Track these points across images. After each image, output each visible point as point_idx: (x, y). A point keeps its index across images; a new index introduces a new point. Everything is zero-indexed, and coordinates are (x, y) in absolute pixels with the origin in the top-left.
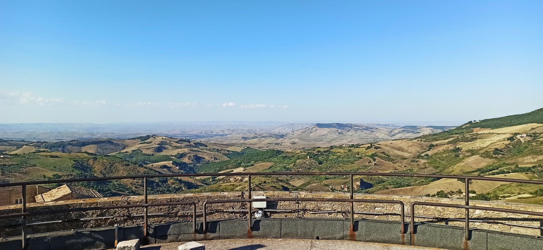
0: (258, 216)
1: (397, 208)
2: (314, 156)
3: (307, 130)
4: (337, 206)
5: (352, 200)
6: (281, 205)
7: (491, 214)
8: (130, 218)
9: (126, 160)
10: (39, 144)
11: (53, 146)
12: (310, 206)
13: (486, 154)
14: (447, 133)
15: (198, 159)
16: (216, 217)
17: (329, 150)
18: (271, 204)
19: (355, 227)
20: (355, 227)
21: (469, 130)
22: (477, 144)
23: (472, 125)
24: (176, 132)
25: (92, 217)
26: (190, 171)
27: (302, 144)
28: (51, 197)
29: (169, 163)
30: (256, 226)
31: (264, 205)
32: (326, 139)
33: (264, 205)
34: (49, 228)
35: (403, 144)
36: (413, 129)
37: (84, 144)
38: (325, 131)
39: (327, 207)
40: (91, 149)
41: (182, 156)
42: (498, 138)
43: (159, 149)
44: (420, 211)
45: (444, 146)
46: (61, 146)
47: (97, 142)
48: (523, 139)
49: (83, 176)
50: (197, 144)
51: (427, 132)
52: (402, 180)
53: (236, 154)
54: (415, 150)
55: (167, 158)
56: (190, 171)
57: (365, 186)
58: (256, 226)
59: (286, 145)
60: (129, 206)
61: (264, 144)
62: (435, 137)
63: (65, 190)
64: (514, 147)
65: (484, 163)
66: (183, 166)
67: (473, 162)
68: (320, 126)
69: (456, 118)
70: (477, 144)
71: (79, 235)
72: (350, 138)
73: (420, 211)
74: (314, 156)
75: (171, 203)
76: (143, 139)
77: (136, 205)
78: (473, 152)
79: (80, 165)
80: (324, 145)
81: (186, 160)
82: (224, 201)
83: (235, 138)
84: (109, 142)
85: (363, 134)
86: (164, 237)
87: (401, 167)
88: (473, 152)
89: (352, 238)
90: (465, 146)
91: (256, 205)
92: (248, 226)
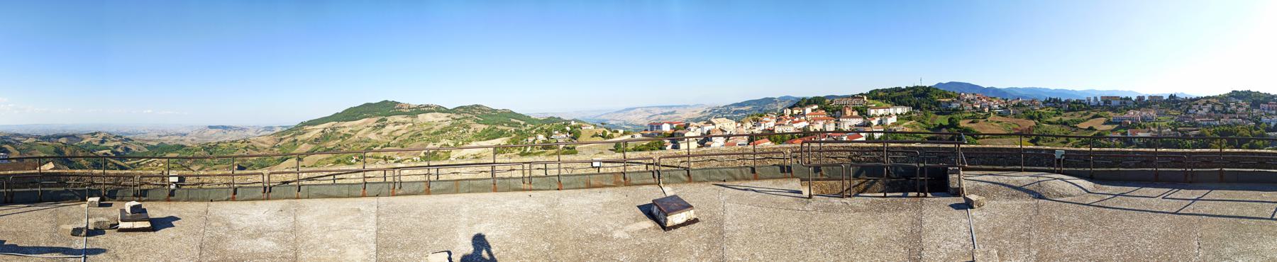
0: (173, 187)
1: (260, 178)
2: (206, 149)
3: (202, 131)
4: (224, 180)
5: (233, 175)
6: (188, 179)
7: (311, 175)
8: (93, 184)
9: (82, 148)
10: (37, 137)
11: (44, 138)
12: (206, 180)
13: (311, 142)
14: (291, 130)
15: (127, 150)
16: (146, 187)
17: (216, 146)
18: (182, 179)
19: (235, 193)
20: (235, 193)
21: (301, 128)
22: (306, 136)
23: (303, 124)
24: (113, 130)
25: (72, 181)
26: (122, 157)
27: (198, 140)
28: (48, 167)
29: (108, 152)
30: (172, 193)
31: (176, 179)
32: (214, 137)
33: (176, 179)
34: (50, 186)
35: (264, 139)
36: (271, 128)
37: (60, 137)
38: (214, 131)
39: (217, 180)
40: (64, 140)
41: (117, 147)
42: (315, 132)
43: (102, 142)
44: (273, 178)
45: (288, 139)
46: (48, 138)
47: (67, 136)
48: (329, 131)
49: (60, 157)
50: (127, 139)
51: (279, 130)
52: (264, 162)
53: (153, 147)
54: (271, 143)
55: (107, 148)
56: (122, 157)
57: (240, 168)
58: (172, 193)
59: (187, 142)
60: (92, 176)
61: (172, 141)
62: (283, 133)
63: (51, 165)
64: (325, 137)
65: (310, 147)
66: (117, 153)
67: (304, 148)
68: (211, 127)
69: (294, 122)
70: (306, 136)
71: (67, 191)
72: (231, 136)
73: (273, 178)
74: (206, 149)
75: (118, 176)
76: (93, 134)
77: (96, 176)
78: (304, 142)
79: (58, 150)
80: (213, 141)
81: (119, 150)
82: (151, 176)
83: (153, 135)
84: (74, 136)
85: (239, 133)
86: (114, 198)
87: (266, 152)
88: (304, 142)
89: (233, 199)
90: (299, 138)
91: (172, 179)
92: (167, 193)
